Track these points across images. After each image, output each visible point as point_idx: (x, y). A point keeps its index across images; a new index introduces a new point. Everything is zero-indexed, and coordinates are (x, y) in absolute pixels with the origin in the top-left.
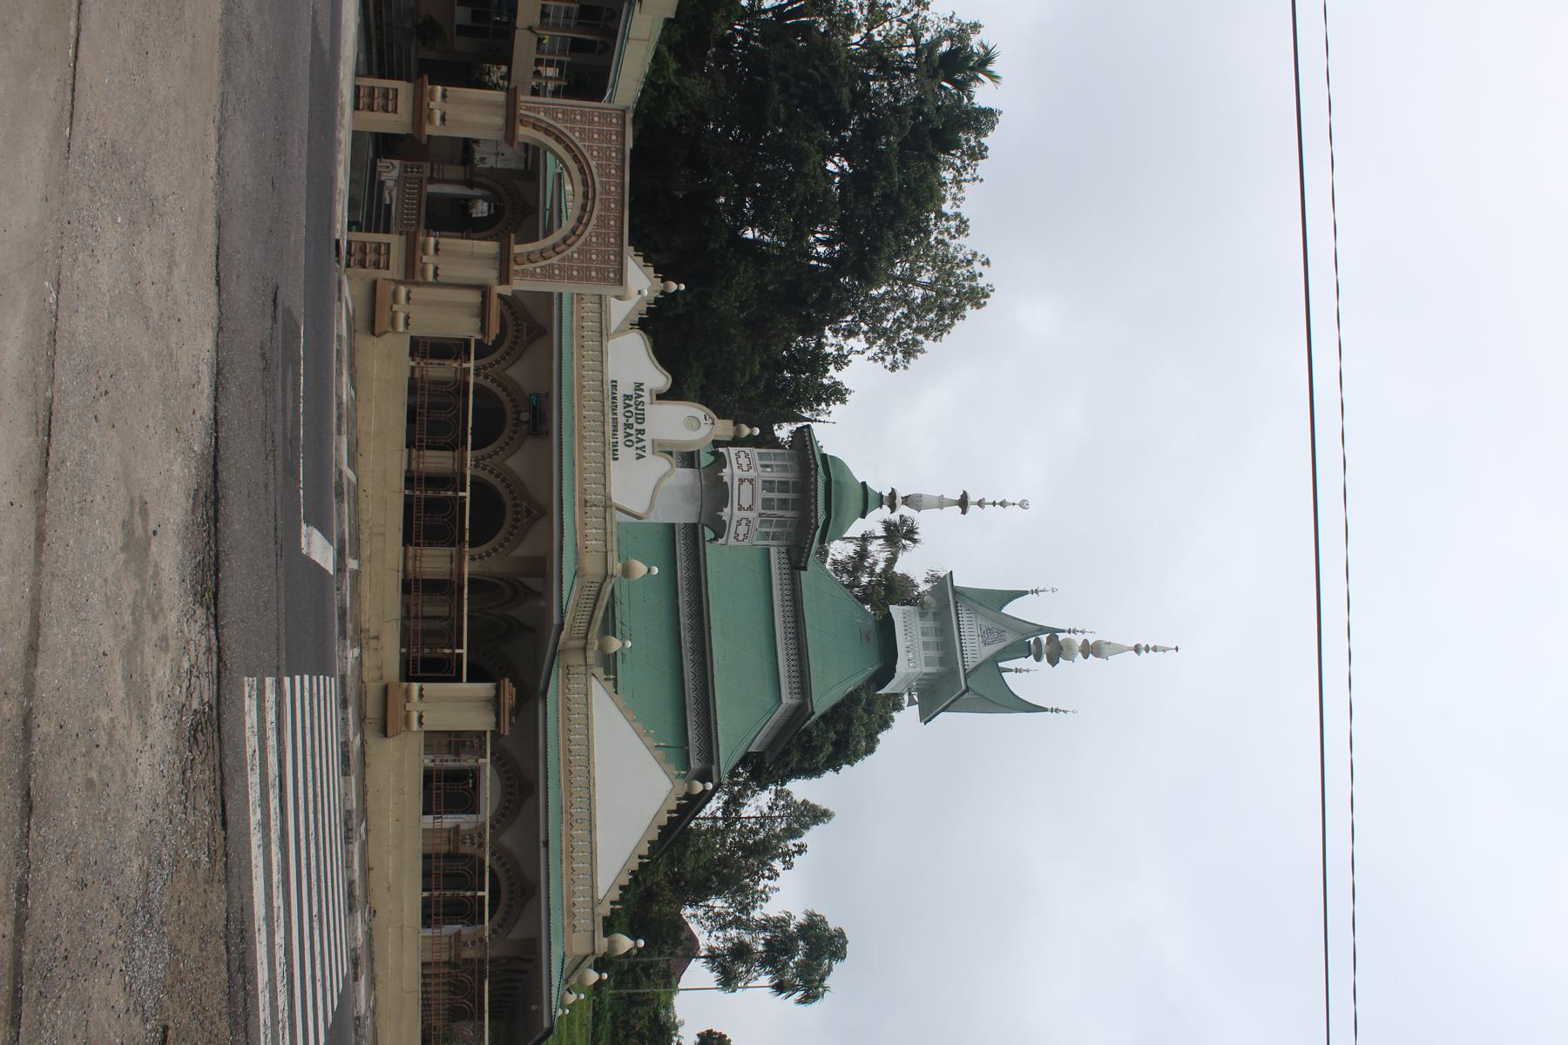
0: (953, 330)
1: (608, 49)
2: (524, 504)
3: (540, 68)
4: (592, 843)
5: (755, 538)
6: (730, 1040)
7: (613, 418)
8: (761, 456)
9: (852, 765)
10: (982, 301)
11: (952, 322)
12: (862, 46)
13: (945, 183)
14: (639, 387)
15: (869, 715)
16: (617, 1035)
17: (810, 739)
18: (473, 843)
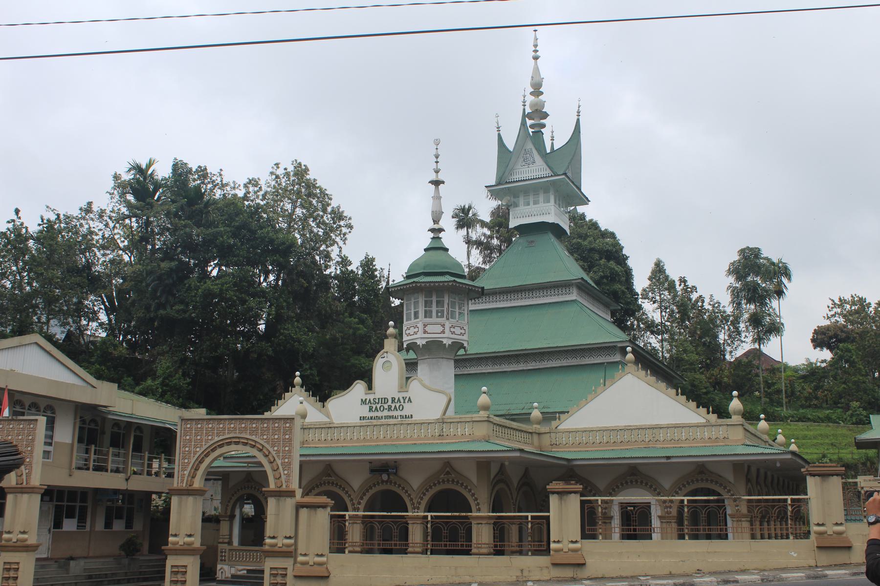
0: (324, 187)
1: (139, 427)
2: (442, 476)
3: (153, 473)
4: (668, 427)
5: (463, 322)
6: (818, 327)
8: (409, 319)
9: (623, 247)
10: (304, 167)
11: (318, 187)
12: (132, 254)
13: (224, 195)
14: (364, 402)
15: (588, 236)
16: (816, 405)
17: (606, 277)
18: (670, 507)
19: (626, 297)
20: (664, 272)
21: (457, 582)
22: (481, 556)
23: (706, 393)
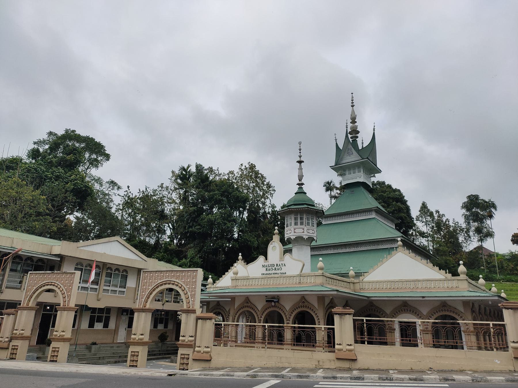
2: (301, 304)
6: (514, 233)
7: (273, 274)
8: (287, 226)
9: (404, 196)
14: (263, 266)
15: (386, 192)
17: (396, 210)
19: (407, 220)
20: (427, 208)
21: (281, 367)
22: (295, 351)
23: (453, 267)
